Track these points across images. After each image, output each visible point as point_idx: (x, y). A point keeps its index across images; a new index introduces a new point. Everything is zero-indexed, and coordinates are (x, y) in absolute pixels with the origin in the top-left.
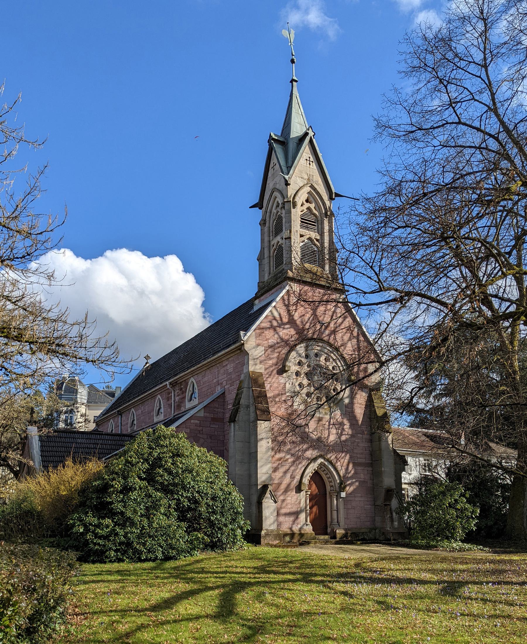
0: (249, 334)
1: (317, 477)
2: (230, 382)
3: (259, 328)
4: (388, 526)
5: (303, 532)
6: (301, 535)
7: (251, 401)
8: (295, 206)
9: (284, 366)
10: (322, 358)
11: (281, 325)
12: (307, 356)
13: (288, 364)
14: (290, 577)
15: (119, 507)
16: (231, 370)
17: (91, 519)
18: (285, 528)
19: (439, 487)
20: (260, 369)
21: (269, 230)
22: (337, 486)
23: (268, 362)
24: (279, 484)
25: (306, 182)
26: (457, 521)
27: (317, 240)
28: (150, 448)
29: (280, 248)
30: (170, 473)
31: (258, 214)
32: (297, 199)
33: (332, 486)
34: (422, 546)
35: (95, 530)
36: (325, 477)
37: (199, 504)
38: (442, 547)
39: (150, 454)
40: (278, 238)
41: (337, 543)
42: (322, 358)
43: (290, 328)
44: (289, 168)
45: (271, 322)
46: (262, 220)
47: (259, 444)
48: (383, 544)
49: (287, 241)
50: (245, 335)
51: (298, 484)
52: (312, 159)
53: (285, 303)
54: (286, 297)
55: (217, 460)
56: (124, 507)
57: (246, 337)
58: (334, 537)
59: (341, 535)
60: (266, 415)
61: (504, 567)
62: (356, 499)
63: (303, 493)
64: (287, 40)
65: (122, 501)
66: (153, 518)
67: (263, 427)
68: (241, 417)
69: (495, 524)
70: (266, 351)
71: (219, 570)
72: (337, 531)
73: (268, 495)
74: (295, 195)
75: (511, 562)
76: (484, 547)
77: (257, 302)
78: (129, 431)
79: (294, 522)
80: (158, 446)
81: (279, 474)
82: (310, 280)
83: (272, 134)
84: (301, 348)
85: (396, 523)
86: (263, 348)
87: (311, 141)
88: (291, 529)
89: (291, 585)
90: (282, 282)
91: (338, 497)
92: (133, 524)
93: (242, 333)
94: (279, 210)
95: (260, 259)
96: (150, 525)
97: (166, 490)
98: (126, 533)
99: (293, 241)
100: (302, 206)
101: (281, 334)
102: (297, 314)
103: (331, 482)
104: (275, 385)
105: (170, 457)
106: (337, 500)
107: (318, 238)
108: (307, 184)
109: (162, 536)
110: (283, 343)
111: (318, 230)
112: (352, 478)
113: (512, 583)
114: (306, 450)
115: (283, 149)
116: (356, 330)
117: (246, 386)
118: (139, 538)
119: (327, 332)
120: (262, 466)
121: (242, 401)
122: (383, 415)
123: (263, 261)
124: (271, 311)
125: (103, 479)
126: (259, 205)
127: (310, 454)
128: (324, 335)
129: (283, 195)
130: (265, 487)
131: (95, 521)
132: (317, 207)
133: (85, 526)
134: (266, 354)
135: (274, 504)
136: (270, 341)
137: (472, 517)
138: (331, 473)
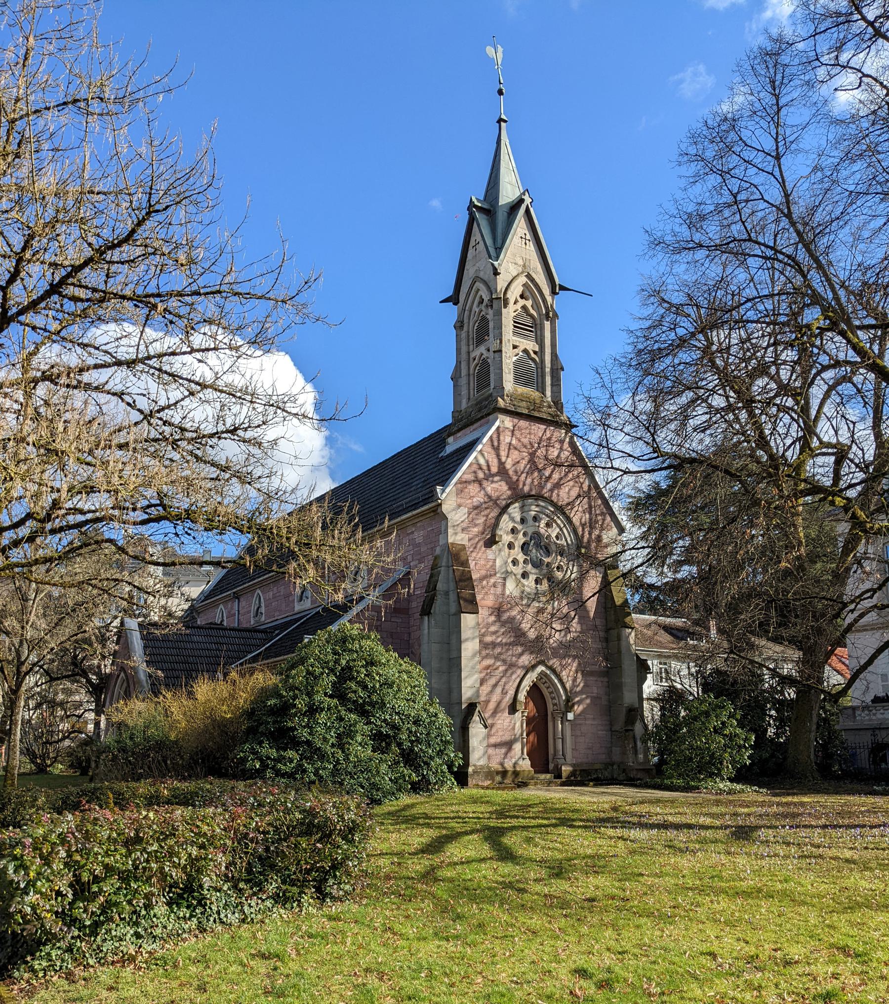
0: (447, 490)
1: (535, 691)
2: (419, 557)
3: (460, 482)
4: (631, 760)
5: (518, 769)
6: (516, 774)
7: (452, 585)
8: (506, 304)
9: (494, 535)
10: (542, 524)
11: (489, 476)
12: (523, 521)
13: (499, 532)
14: (545, 822)
15: (304, 734)
16: (419, 540)
17: (268, 750)
18: (495, 765)
19: (700, 704)
20: (462, 539)
21: (468, 336)
22: (563, 704)
23: (472, 529)
24: (487, 702)
25: (520, 269)
26: (725, 751)
27: (535, 353)
28: (335, 653)
29: (484, 365)
30: (365, 687)
31: (452, 311)
32: (508, 296)
33: (555, 705)
34: (679, 787)
35: (274, 766)
36: (545, 692)
37: (399, 730)
38: (706, 788)
39: (337, 662)
40: (482, 349)
41: (563, 784)
42: (542, 524)
43: (501, 481)
44: (499, 249)
45: (475, 472)
46: (457, 321)
47: (463, 646)
48: (626, 785)
49: (497, 355)
50: (443, 491)
51: (511, 701)
52: (528, 237)
53: (493, 445)
54: (495, 436)
55: (416, 670)
56: (310, 734)
57: (444, 495)
58: (558, 776)
59: (568, 772)
60: (472, 606)
61: (796, 810)
62: (587, 722)
63: (518, 715)
64: (492, 61)
65: (307, 726)
66: (349, 749)
67: (468, 620)
68: (437, 608)
69: (772, 756)
70: (469, 514)
71: (443, 815)
72: (563, 768)
73: (476, 718)
74: (506, 289)
75: (802, 804)
76: (760, 787)
77: (450, 440)
78: (252, 623)
79: (506, 754)
80: (344, 651)
81: (485, 689)
82: (526, 411)
83: (474, 199)
84: (515, 510)
85: (641, 756)
86: (466, 510)
87: (527, 211)
88: (502, 764)
89: (554, 830)
90: (489, 414)
91: (564, 719)
92: (323, 757)
93: (439, 489)
94: (483, 309)
95: (455, 378)
96: (347, 759)
97: (362, 711)
98: (317, 770)
99: (504, 354)
100: (515, 303)
101: (489, 489)
102: (509, 460)
103: (553, 698)
104: (482, 562)
105: (362, 666)
106: (562, 724)
107: (537, 349)
108: (522, 273)
109: (362, 772)
110: (491, 504)
111: (536, 335)
112: (581, 692)
113: (812, 827)
114: (521, 654)
115: (488, 220)
116: (587, 483)
117: (444, 564)
118: (334, 776)
119: (549, 486)
120: (466, 677)
121: (440, 586)
122: (622, 604)
123: (460, 380)
124: (476, 458)
125: (281, 696)
126: (454, 299)
127: (526, 660)
128: (545, 490)
129: (491, 290)
130: (472, 706)
131: (274, 753)
132: (536, 305)
133: (261, 760)
134: (470, 519)
135: (484, 730)
136: (475, 500)
137: (745, 746)
138: (554, 685)
